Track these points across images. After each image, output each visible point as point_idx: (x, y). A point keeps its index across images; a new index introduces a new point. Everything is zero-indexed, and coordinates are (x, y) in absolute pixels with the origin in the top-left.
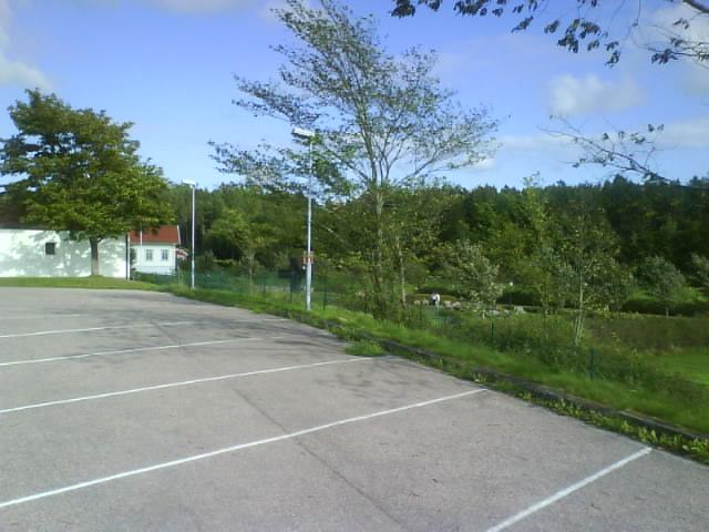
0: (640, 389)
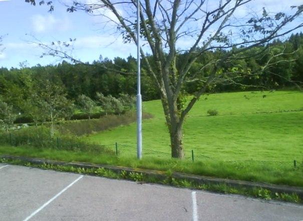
0: (79, 151)
